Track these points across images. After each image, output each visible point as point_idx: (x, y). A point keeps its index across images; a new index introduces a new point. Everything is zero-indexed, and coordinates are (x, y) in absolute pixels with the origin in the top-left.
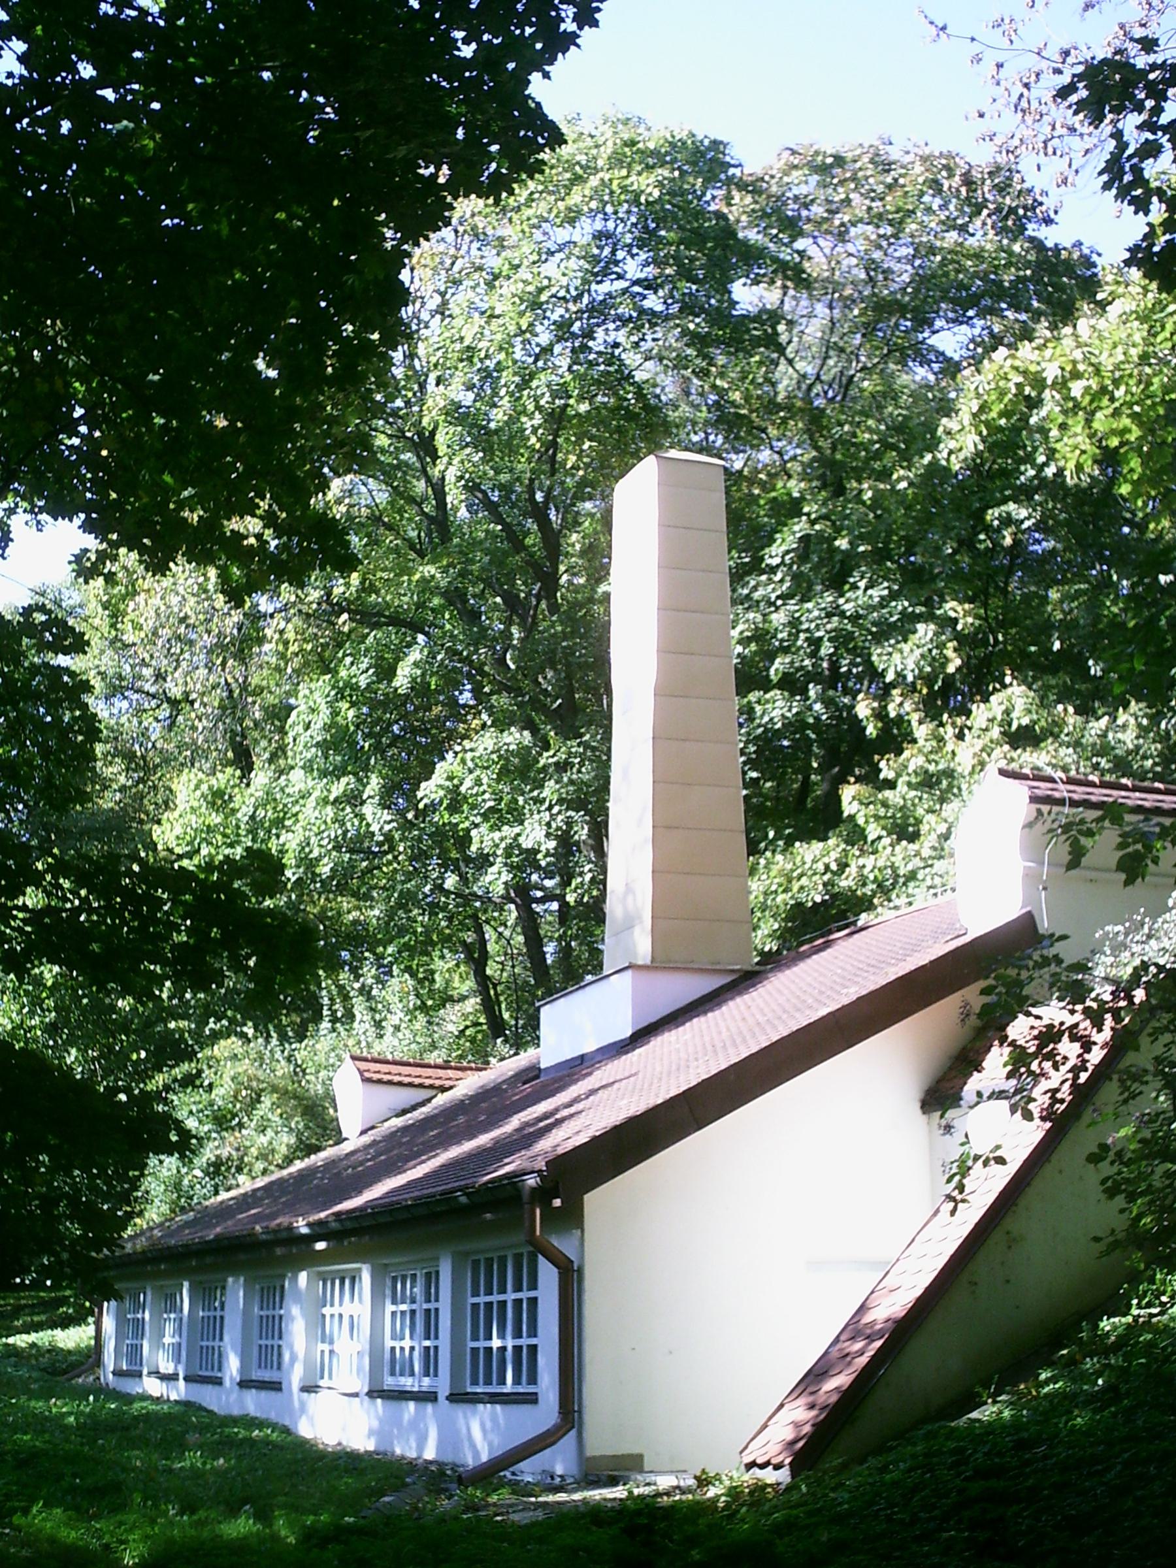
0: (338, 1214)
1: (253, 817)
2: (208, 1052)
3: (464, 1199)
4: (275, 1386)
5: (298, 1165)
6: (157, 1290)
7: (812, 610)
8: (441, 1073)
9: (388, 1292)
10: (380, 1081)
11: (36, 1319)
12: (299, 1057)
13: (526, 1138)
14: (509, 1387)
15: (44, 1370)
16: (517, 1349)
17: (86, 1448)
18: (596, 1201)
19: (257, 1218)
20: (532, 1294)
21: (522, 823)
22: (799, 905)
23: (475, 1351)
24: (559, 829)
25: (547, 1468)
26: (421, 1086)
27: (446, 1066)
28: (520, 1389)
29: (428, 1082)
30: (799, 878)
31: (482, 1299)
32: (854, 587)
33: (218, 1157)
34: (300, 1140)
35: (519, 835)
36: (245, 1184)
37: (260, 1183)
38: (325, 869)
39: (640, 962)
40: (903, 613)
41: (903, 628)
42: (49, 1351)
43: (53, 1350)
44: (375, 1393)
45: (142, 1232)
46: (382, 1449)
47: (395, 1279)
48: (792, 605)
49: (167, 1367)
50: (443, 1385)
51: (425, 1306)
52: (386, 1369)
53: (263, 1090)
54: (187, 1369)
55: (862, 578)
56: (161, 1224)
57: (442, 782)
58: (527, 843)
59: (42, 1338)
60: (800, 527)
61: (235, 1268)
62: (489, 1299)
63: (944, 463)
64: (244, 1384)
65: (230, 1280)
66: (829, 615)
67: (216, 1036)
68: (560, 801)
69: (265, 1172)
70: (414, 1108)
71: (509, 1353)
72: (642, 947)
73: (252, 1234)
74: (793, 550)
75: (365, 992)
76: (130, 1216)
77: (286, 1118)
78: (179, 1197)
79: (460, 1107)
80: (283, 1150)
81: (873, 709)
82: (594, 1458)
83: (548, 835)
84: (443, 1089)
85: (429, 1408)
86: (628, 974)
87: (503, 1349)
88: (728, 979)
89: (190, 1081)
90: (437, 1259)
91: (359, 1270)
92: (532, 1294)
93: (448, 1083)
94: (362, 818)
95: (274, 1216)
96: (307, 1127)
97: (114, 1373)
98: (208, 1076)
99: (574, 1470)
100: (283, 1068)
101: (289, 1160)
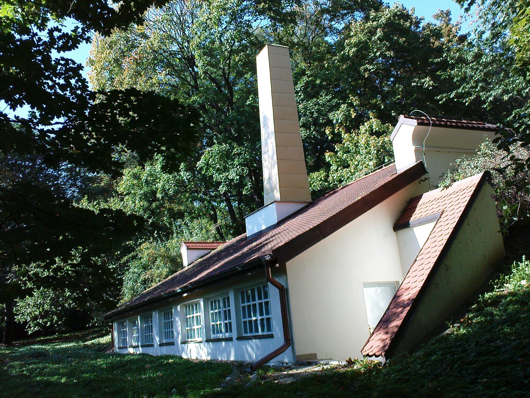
0: (190, 283)
1: (147, 180)
2: (139, 248)
3: (240, 269)
4: (172, 344)
5: (170, 277)
6: (129, 321)
7: (310, 103)
8: (212, 244)
9: (210, 307)
10: (193, 249)
11: (94, 336)
12: (168, 245)
13: (258, 249)
14: (260, 333)
15: (97, 350)
16: (262, 320)
17: (110, 375)
18: (289, 264)
19: (160, 292)
20: (266, 300)
21: (228, 171)
22: (314, 191)
23: (245, 322)
24: (240, 172)
25: (280, 360)
26: (206, 249)
27: (213, 243)
28: (265, 333)
29: (208, 247)
30: (313, 183)
31: (246, 304)
32: (322, 96)
33: (145, 278)
34: (170, 270)
35: (228, 175)
36: (154, 285)
37: (158, 284)
38: (171, 192)
39: (278, 200)
40: (336, 102)
41: (337, 107)
42: (98, 344)
43: (99, 344)
44: (208, 341)
45: (123, 304)
46: (213, 359)
47: (212, 303)
48: (305, 103)
49: (134, 344)
50: (234, 335)
51: (224, 309)
52: (212, 333)
53: (157, 257)
54: (141, 343)
55: (324, 93)
56: (129, 301)
57: (203, 162)
58: (230, 177)
59: (95, 341)
60: (305, 78)
61: (154, 309)
62: (249, 304)
63: (347, 54)
64: (161, 345)
65: (154, 313)
66: (315, 105)
67: (141, 244)
68: (239, 165)
69: (159, 281)
70: (204, 256)
71: (259, 322)
72: (277, 195)
73: (161, 296)
74: (303, 86)
75: (186, 224)
76: (119, 300)
77: (165, 264)
78: (134, 292)
79: (221, 251)
80: (165, 273)
81: (330, 131)
82: (299, 356)
83: (236, 175)
84: (213, 249)
85: (230, 343)
86: (274, 204)
87: (256, 320)
88: (300, 206)
89: (134, 257)
90: (228, 293)
91: (199, 301)
92: (266, 300)
93: (214, 247)
94: (180, 175)
95: (166, 290)
96: (172, 266)
97: (118, 348)
98: (140, 255)
99: (292, 360)
100: (163, 250)
101: (167, 276)
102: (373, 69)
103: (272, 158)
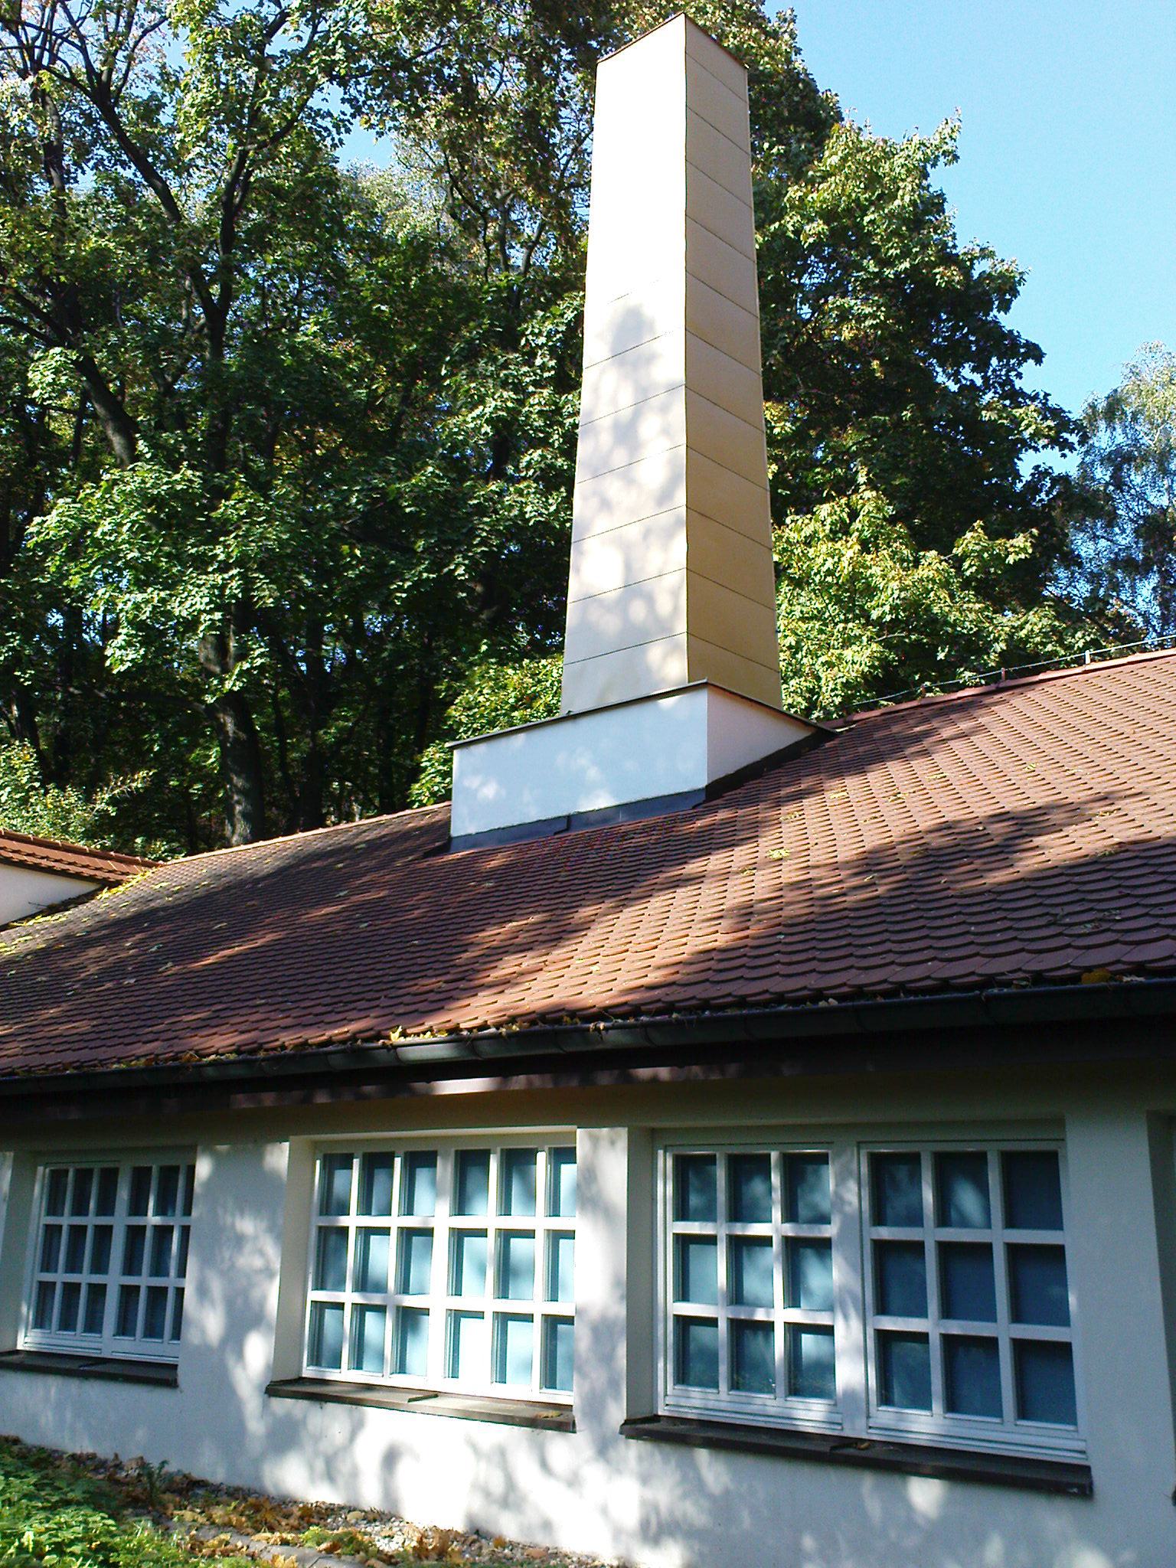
8: (99, 863)
26: (78, 876)
90: (1059, 1123)
93: (113, 877)
102: (874, 316)
103: (664, 497)
